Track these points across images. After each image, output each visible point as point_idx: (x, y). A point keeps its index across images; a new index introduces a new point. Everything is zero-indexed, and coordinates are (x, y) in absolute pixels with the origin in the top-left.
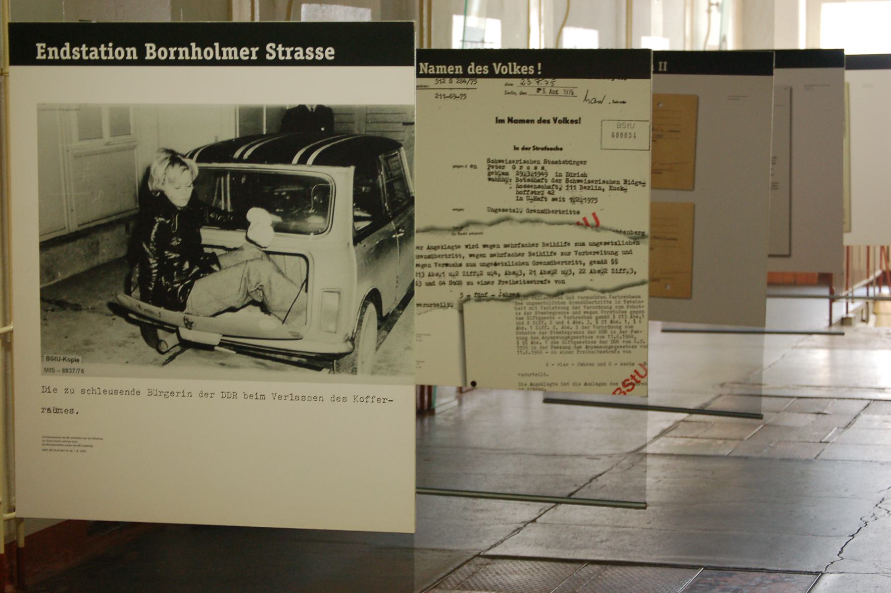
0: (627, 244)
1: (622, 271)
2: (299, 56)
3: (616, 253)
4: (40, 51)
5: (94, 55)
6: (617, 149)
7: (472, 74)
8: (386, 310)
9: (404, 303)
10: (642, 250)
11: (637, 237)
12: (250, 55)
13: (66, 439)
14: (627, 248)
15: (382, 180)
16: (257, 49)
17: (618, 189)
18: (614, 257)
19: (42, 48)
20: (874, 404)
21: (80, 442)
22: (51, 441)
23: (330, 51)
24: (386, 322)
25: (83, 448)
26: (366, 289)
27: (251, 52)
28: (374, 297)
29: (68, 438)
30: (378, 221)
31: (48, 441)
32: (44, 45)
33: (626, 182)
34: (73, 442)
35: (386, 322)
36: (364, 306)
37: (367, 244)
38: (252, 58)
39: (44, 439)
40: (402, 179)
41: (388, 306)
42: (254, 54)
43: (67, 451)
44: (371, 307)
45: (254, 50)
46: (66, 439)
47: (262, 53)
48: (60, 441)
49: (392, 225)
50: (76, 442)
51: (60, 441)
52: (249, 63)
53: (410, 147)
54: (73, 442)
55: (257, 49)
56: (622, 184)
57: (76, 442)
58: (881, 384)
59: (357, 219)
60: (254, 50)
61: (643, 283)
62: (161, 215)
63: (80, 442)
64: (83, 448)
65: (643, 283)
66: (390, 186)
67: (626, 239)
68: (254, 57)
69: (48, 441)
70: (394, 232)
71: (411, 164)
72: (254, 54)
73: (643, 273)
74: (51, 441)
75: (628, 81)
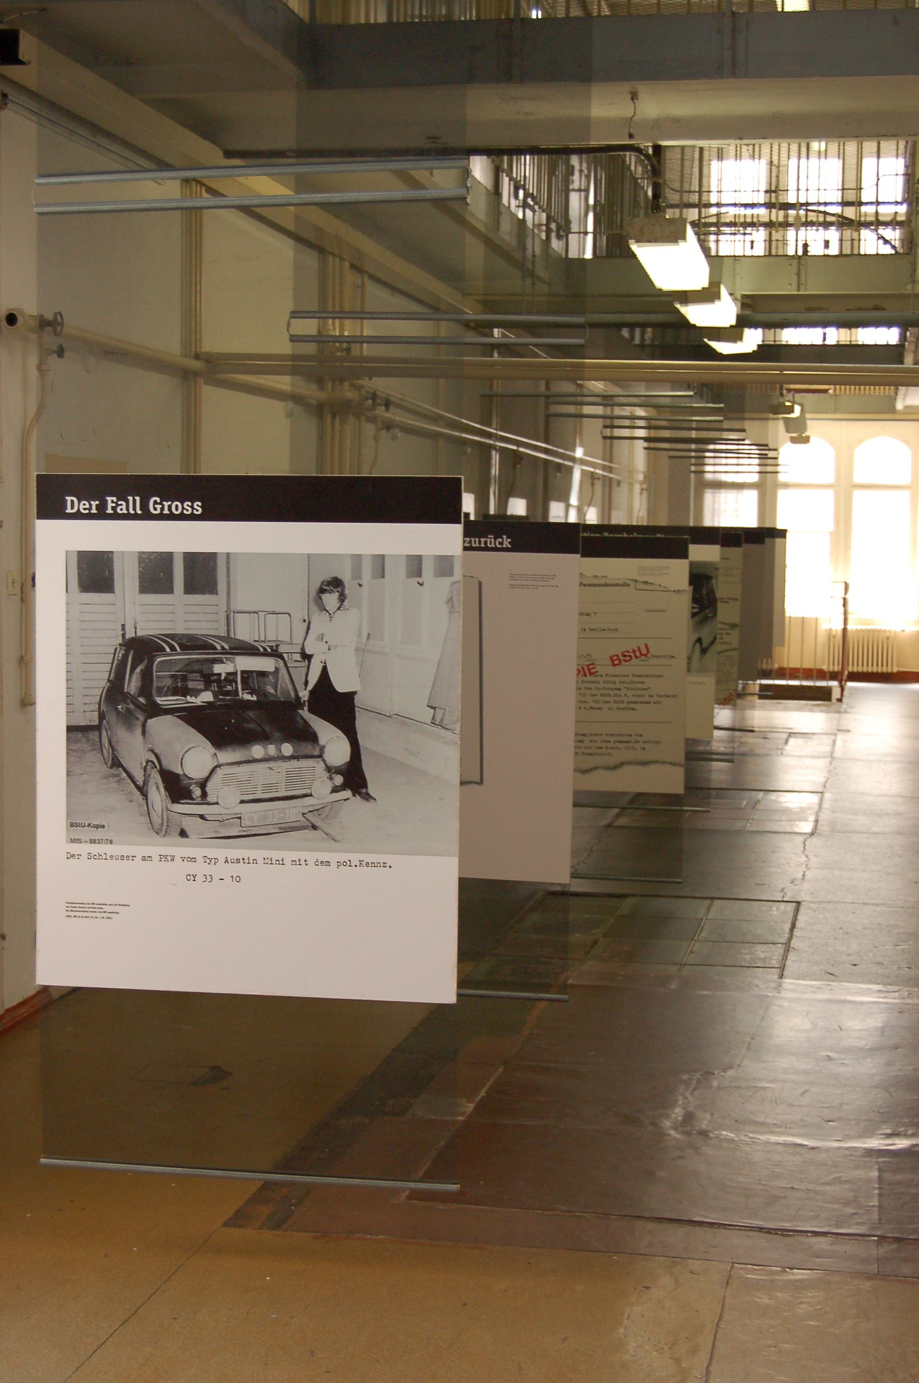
0: (728, 630)
1: (725, 643)
2: (121, 510)
3: (722, 634)
4: (110, 505)
5: (122, 509)
6: (277, 624)
7: (492, 547)
8: (704, 645)
9: (712, 643)
10: (735, 633)
11: (733, 626)
12: (90, 509)
13: (91, 906)
14: (728, 631)
15: (704, 592)
16: (97, 502)
17: (724, 602)
18: (721, 636)
19: (113, 502)
20: (792, 735)
21: (106, 908)
22: (75, 907)
23: (84, 504)
24: (704, 651)
25: (109, 915)
26: (696, 637)
27: (91, 505)
28: (699, 640)
29: (93, 904)
30: (702, 608)
31: (72, 907)
32: (115, 499)
33: (728, 598)
34: (99, 908)
35: (704, 651)
36: (695, 644)
37: (697, 619)
38: (92, 512)
39: (68, 905)
40: (713, 591)
41: (705, 644)
42: (94, 507)
43: (92, 917)
44: (698, 645)
45: (94, 504)
46: (91, 906)
47: (102, 507)
48: (85, 908)
49: (708, 611)
50: (102, 908)
51: (85, 908)
52: (89, 516)
53: (717, 579)
54: (99, 908)
55: (97, 502)
56: (726, 600)
57: (102, 908)
58: (789, 726)
59: (693, 608)
60: (94, 504)
61: (735, 649)
62: (696, 595)
63: (106, 908)
64: (109, 915)
65: (735, 649)
66: (708, 595)
67: (726, 627)
68: (94, 511)
69: (72, 907)
70: (709, 613)
71: (717, 584)
72: (94, 507)
73: (736, 644)
74: (75, 907)
75: (788, 562)
